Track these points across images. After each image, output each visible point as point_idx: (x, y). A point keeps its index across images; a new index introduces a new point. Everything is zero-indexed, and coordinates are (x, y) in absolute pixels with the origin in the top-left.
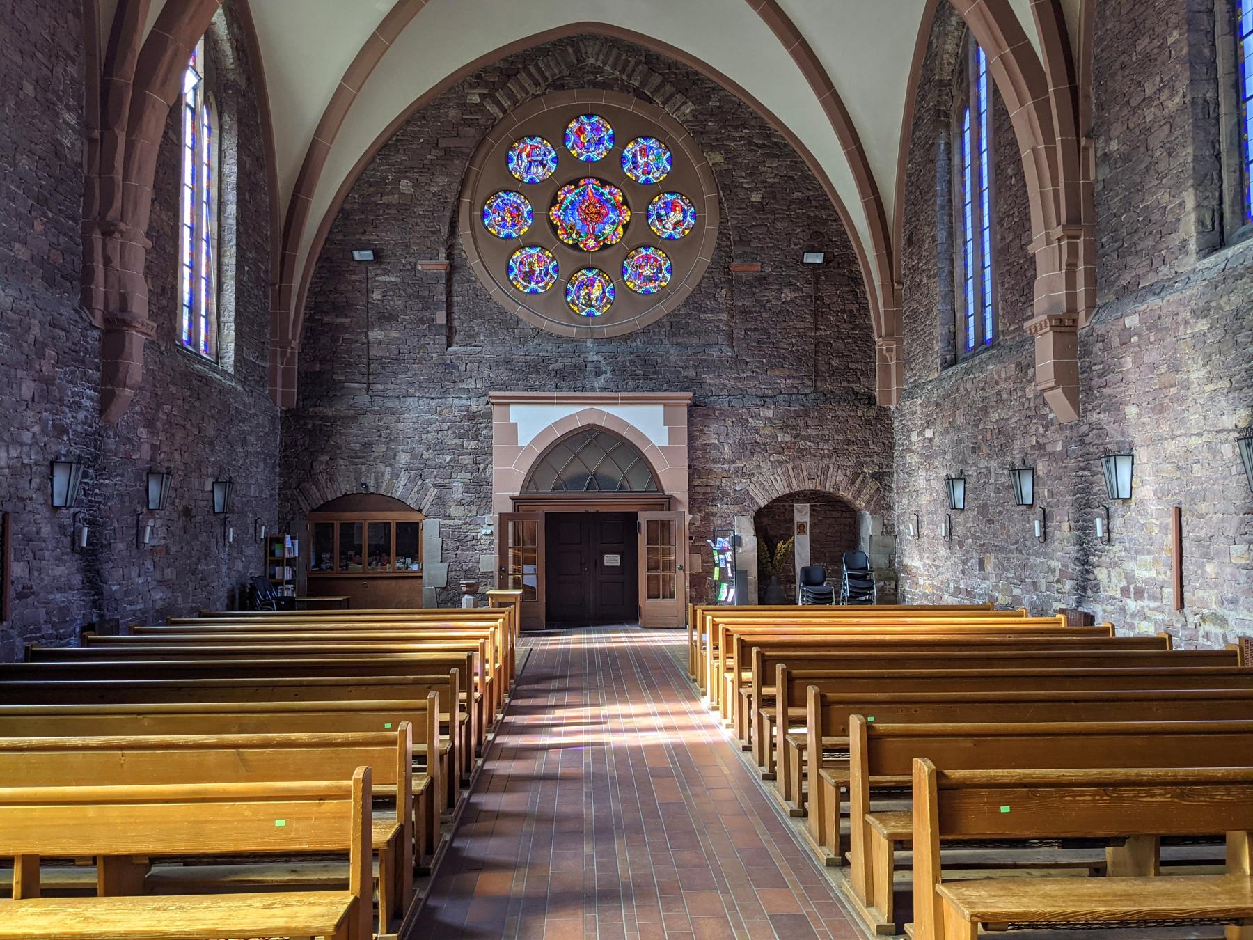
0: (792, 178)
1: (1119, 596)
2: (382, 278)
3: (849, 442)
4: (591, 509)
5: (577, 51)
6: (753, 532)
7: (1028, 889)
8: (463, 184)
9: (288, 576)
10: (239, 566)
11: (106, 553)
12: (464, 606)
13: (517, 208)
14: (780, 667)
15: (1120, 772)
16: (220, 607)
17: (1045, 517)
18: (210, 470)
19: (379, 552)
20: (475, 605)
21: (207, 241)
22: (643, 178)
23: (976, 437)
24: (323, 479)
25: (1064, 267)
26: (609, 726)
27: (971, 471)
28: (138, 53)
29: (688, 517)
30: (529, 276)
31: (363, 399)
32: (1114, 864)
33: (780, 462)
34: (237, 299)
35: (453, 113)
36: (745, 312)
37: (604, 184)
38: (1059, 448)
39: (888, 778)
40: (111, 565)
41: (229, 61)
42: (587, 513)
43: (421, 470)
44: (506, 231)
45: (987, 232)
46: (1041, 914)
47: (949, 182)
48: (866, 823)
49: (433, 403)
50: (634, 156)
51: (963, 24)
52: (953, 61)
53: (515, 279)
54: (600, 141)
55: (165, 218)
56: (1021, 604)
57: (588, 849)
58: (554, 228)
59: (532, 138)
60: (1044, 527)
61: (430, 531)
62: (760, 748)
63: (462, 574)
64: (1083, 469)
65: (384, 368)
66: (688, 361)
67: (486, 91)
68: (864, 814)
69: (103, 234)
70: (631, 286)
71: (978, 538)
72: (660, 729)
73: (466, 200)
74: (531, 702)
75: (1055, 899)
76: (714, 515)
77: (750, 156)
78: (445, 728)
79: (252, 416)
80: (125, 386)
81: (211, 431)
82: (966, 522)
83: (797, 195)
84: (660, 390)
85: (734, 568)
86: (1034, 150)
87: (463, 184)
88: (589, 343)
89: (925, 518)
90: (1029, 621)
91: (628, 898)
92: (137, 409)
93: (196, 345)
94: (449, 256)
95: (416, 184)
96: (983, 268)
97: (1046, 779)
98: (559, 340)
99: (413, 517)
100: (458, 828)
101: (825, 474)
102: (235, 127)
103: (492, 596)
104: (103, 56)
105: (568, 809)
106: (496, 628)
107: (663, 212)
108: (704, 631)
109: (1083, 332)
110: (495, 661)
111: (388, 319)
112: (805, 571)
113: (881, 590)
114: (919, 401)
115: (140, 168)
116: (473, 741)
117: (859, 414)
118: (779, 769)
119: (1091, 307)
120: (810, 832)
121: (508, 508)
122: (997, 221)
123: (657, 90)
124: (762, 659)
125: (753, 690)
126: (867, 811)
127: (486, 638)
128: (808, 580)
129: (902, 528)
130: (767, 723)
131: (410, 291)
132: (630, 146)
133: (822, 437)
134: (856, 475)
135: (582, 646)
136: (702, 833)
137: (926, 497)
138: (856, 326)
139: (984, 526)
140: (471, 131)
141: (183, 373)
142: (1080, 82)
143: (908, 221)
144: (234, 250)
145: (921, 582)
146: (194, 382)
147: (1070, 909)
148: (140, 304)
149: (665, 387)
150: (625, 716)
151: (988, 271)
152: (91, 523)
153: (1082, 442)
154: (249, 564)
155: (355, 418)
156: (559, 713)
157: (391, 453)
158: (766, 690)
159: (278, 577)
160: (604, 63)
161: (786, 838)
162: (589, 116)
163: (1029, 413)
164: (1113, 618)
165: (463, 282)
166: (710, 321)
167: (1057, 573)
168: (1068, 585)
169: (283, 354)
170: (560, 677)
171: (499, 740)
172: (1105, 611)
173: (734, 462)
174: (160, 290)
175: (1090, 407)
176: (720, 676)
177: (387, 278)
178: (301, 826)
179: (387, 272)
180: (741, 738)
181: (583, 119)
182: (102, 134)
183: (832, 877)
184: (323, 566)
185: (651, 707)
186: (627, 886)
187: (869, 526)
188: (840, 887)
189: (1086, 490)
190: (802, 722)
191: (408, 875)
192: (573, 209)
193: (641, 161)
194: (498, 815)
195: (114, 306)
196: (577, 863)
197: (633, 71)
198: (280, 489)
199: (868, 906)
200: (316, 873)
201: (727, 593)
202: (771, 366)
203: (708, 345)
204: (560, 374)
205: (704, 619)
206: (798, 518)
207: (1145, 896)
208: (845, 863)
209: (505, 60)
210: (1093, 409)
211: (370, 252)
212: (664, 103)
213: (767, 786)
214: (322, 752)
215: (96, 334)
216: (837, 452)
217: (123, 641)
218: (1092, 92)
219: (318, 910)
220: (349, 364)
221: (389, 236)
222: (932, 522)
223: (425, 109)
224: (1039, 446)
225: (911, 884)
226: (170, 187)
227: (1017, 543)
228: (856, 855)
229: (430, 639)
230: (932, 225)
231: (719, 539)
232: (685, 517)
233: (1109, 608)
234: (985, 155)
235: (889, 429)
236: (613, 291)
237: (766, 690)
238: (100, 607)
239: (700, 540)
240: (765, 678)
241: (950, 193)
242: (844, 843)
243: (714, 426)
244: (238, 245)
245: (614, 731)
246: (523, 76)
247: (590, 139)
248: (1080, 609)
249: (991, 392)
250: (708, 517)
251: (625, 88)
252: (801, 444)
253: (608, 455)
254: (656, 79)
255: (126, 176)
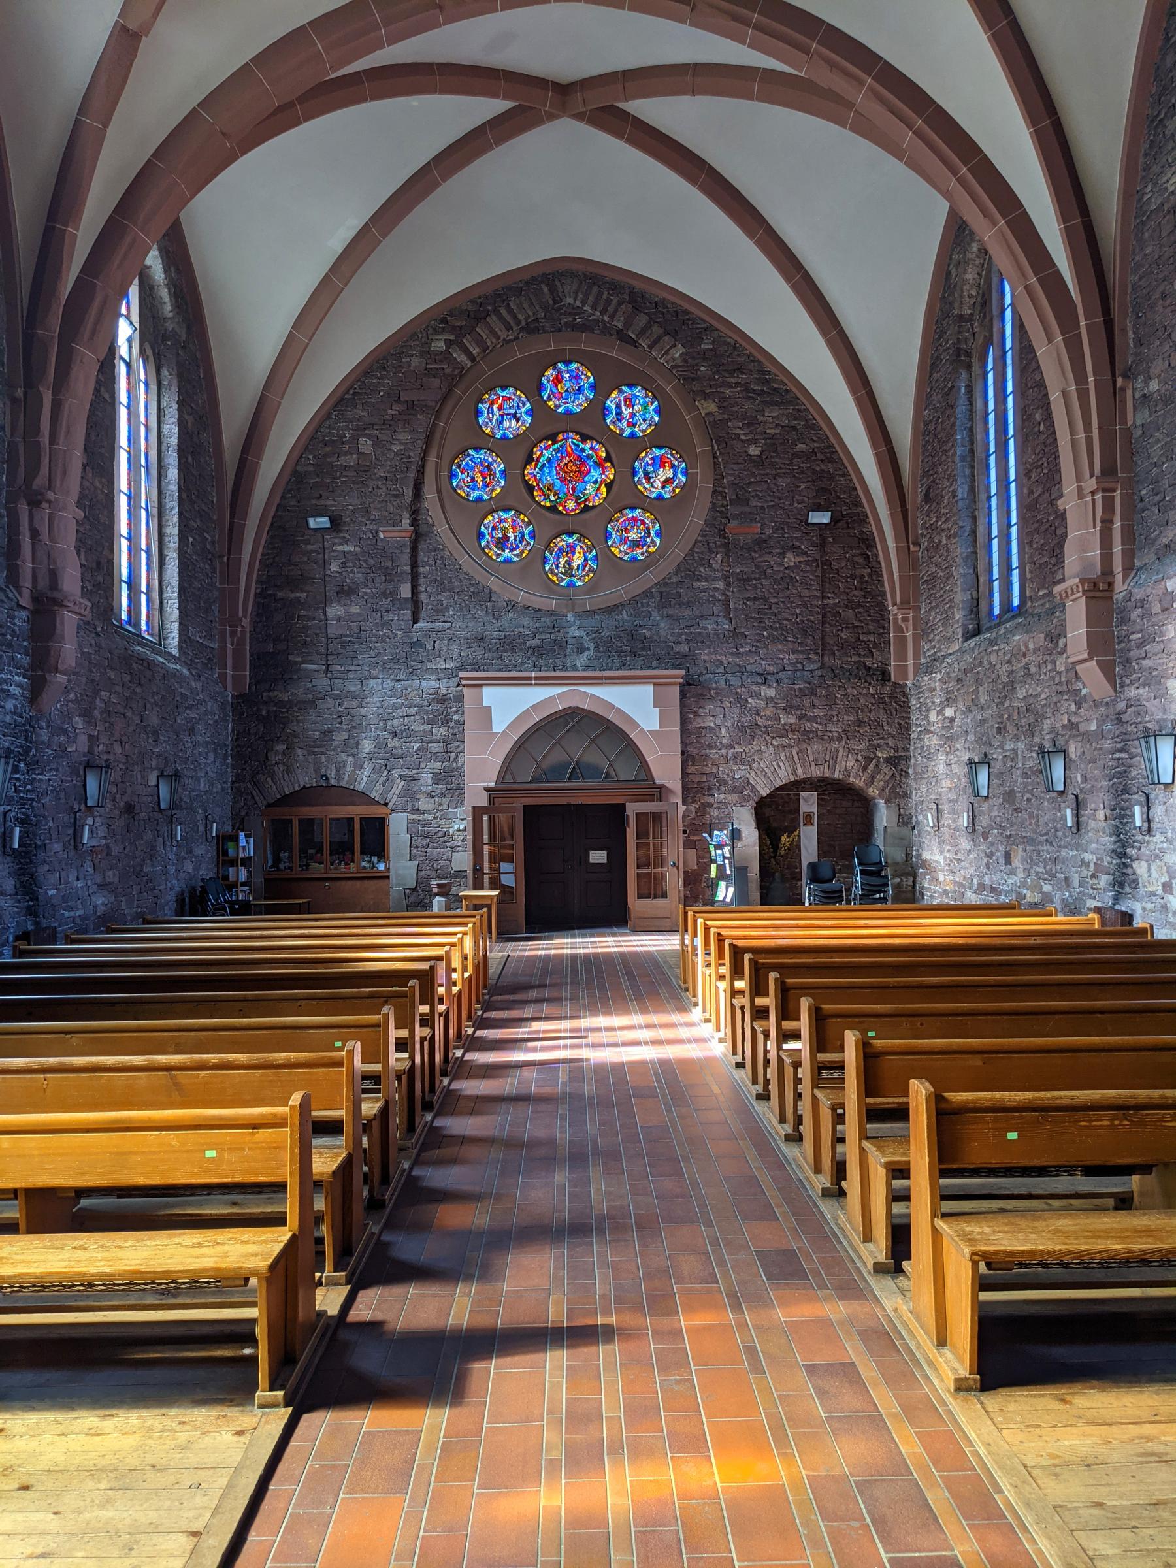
0: (794, 428)
1: (1160, 892)
2: (340, 548)
3: (860, 723)
4: (574, 801)
5: (553, 290)
6: (753, 824)
7: (1036, 1224)
8: (428, 441)
9: (243, 877)
10: (189, 866)
11: (41, 854)
12: (435, 909)
13: (489, 468)
14: (773, 976)
15: (1142, 1094)
16: (168, 912)
17: (1078, 806)
18: (154, 763)
19: (343, 850)
20: (448, 908)
21: (147, 511)
22: (628, 431)
23: (1001, 716)
24: (279, 770)
25: (1098, 524)
26: (590, 1040)
27: (996, 754)
28: (63, 301)
29: (682, 808)
30: (502, 543)
31: (322, 682)
32: (1141, 1194)
33: (784, 747)
34: (181, 573)
35: (416, 362)
36: (743, 580)
37: (584, 438)
38: (1093, 727)
39: (891, 1100)
40: (46, 868)
41: (167, 308)
42: (569, 805)
43: (386, 759)
44: (477, 493)
45: (1013, 486)
46: (1050, 1253)
47: (971, 429)
48: (862, 1151)
49: (398, 685)
50: (618, 406)
51: (984, 251)
52: (974, 292)
53: (487, 546)
54: (580, 390)
55: (97, 484)
56: (1052, 902)
57: (561, 1177)
58: (530, 489)
59: (504, 388)
60: (1077, 815)
61: (398, 826)
62: (753, 1064)
63: (433, 874)
64: (1121, 751)
65: (344, 648)
66: (680, 635)
67: (452, 337)
68: (860, 1140)
69: (29, 505)
70: (616, 552)
71: (1004, 829)
72: (646, 1043)
73: (432, 459)
74: (506, 1014)
75: (1066, 1235)
76: (710, 805)
77: (747, 405)
78: (402, 1045)
79: (200, 702)
80: (57, 671)
81: (154, 720)
82: (990, 811)
83: (800, 447)
84: (649, 668)
85: (732, 864)
86: (1064, 393)
87: (428, 441)
88: (570, 616)
89: (945, 807)
90: (1059, 921)
91: (601, 1232)
92: (72, 696)
93: (137, 625)
94: (414, 522)
95: (376, 442)
96: (1009, 526)
97: (1058, 1102)
98: (537, 614)
99: (379, 811)
100: (418, 1155)
101: (834, 758)
102: (175, 382)
103: (466, 897)
104: (25, 306)
105: (541, 1134)
106: (465, 933)
107: (650, 469)
108: (695, 935)
109: (1120, 597)
110: (465, 970)
111: (346, 592)
112: (813, 867)
113: (897, 887)
114: (939, 676)
115: (68, 432)
116: (438, 1058)
117: (872, 691)
118: (774, 1088)
119: (1128, 568)
120: (805, 1159)
121: (483, 801)
122: (1025, 473)
123: (642, 332)
124: (754, 966)
125: (745, 1001)
126: (864, 1136)
127: (453, 945)
128: (815, 878)
129: (920, 817)
130: (760, 1037)
131: (371, 562)
132: (614, 395)
133: (830, 718)
134: (869, 760)
135: (565, 951)
136: (686, 1159)
137: (946, 784)
138: (867, 593)
139: (1011, 814)
140: (436, 382)
141: (123, 658)
142: (1116, 313)
143: (926, 474)
144: (176, 519)
145: (941, 877)
146: (134, 665)
147: (1083, 1247)
148: (71, 581)
149: (655, 664)
150: (608, 1029)
151: (1014, 530)
152: (24, 822)
153: (1119, 721)
154: (198, 865)
155: (313, 703)
156: (536, 1026)
157: (352, 741)
158: (760, 1001)
159: (232, 878)
160: (584, 303)
161: (778, 1165)
162: (567, 363)
163: (1060, 689)
164: (1153, 918)
165: (430, 551)
166: (704, 591)
167: (1092, 866)
168: (1104, 880)
169: (233, 633)
170: (539, 986)
171: (469, 1056)
172: (1144, 909)
173: (732, 747)
174: (94, 565)
175: (1127, 681)
176: (712, 983)
177: (346, 548)
178: (233, 1157)
179: (346, 541)
180: (734, 1053)
181: (561, 366)
182: (25, 394)
183: (827, 1208)
184: (282, 866)
185: (637, 1019)
186: (601, 1219)
187: (884, 817)
188: (836, 1219)
189: (1124, 775)
190: (796, 1036)
191: (358, 1209)
192: (551, 467)
193: (626, 412)
194: (463, 1140)
195: (43, 584)
196: (546, 1193)
197: (616, 311)
198: (233, 782)
199: (865, 1241)
200: (258, 1206)
201: (725, 892)
202: (773, 640)
203: (703, 617)
204: (538, 652)
205: (695, 922)
206: (804, 808)
207: (1167, 1231)
208: (842, 1193)
209: (472, 302)
210: (1132, 683)
211: (326, 519)
212: (651, 347)
213: (760, 1108)
214: (262, 1075)
215: (24, 614)
216: (847, 734)
217: (62, 951)
218: (1129, 325)
219: (252, 1248)
220: (305, 643)
221: (347, 501)
222: (953, 811)
223: (384, 358)
224: (1072, 726)
225: (908, 1216)
226: (103, 450)
227: (1047, 833)
228: (852, 1184)
229: (395, 947)
230: (952, 478)
231: (716, 833)
232: (678, 808)
233: (1149, 906)
234: (1010, 399)
235: (905, 708)
236: (596, 558)
237: (760, 1001)
238: (36, 915)
239: (696, 833)
240: (758, 988)
241: (972, 442)
242: (840, 1170)
243: (709, 707)
244: (180, 513)
245: (595, 1046)
246: (493, 320)
247: (569, 388)
248: (1118, 907)
249: (1018, 666)
250: (703, 808)
251: (606, 331)
252: (807, 726)
253: (593, 741)
254: (642, 320)
255: (53, 440)
